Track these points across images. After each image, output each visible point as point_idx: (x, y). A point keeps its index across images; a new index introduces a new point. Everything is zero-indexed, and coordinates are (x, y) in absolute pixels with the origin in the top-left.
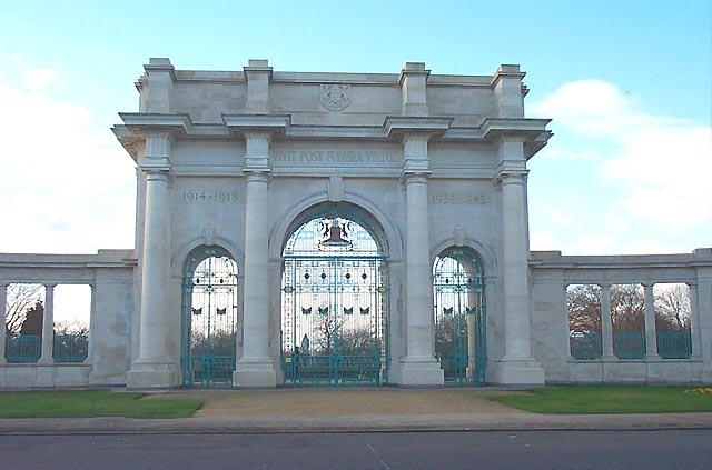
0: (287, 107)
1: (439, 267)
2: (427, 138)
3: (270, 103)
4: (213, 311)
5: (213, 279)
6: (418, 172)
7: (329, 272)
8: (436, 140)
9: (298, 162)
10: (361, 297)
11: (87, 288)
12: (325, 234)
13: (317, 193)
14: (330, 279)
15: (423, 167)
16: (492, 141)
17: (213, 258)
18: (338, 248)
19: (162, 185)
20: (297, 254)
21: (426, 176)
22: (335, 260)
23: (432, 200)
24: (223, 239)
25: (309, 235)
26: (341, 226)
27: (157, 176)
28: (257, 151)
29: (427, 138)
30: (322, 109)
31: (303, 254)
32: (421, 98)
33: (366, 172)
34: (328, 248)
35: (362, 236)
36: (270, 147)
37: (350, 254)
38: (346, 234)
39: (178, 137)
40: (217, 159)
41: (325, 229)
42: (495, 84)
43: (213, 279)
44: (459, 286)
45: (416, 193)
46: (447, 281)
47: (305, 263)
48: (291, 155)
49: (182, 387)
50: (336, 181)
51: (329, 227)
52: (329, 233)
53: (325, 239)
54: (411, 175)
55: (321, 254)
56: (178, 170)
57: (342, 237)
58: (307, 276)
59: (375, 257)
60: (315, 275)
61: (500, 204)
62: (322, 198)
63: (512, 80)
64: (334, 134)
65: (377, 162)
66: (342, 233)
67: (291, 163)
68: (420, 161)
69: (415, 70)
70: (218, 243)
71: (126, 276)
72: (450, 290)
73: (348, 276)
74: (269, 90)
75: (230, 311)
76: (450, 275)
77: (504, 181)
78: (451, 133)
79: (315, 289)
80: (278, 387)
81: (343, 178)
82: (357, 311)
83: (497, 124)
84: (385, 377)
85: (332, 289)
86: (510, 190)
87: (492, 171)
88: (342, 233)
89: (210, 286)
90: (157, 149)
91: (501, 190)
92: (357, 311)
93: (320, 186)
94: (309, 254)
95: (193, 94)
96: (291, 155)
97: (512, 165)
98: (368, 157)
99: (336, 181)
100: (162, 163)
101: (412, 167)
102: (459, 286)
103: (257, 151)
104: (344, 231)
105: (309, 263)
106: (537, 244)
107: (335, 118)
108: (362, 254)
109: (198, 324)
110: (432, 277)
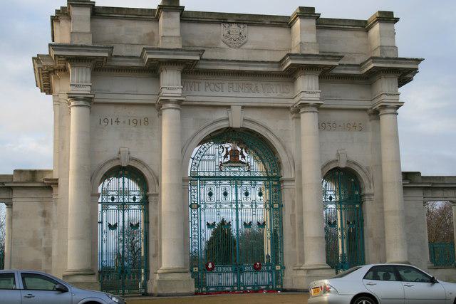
0: (198, 43)
2: (182, 68)
3: (183, 36)
5: (126, 198)
6: (312, 103)
8: (326, 75)
9: (205, 92)
10: (258, 212)
12: (226, 157)
13: (219, 120)
14: (232, 197)
15: (315, 98)
16: (368, 78)
17: (126, 179)
18: (237, 169)
19: (86, 110)
20: (202, 174)
21: (317, 106)
22: (237, 180)
23: (322, 126)
24: (136, 160)
25: (211, 157)
27: (81, 103)
28: (171, 81)
29: (182, 68)
30: (223, 45)
31: (207, 174)
32: (311, 37)
33: (263, 102)
36: (182, 78)
37: (247, 174)
38: (244, 157)
39: (101, 66)
40: (136, 90)
41: (225, 152)
42: (370, 27)
45: (308, 120)
47: (209, 183)
48: (197, 84)
49: (196, 293)
50: (236, 110)
51: (229, 150)
52: (229, 156)
53: (226, 160)
54: (167, 101)
55: (223, 174)
56: (98, 98)
57: (240, 159)
58: (225, 194)
61: (377, 131)
62: (224, 125)
64: (237, 68)
65: (273, 94)
66: (240, 156)
67: (196, 93)
68: (313, 93)
69: (307, 13)
70: (132, 164)
71: (43, 195)
73: (210, 194)
74: (91, 20)
77: (382, 112)
78: (203, 64)
80: (196, 293)
81: (243, 107)
83: (379, 62)
84: (145, 286)
86: (386, 119)
87: (370, 103)
88: (240, 156)
89: (124, 204)
90: (78, 79)
91: (300, 118)
93: (221, 114)
95: (110, 28)
96: (197, 84)
97: (389, 97)
98: (264, 89)
99: (236, 110)
100: (86, 90)
101: (166, 93)
103: (171, 81)
104: (242, 154)
105: (211, 182)
106: (407, 167)
107: (234, 54)
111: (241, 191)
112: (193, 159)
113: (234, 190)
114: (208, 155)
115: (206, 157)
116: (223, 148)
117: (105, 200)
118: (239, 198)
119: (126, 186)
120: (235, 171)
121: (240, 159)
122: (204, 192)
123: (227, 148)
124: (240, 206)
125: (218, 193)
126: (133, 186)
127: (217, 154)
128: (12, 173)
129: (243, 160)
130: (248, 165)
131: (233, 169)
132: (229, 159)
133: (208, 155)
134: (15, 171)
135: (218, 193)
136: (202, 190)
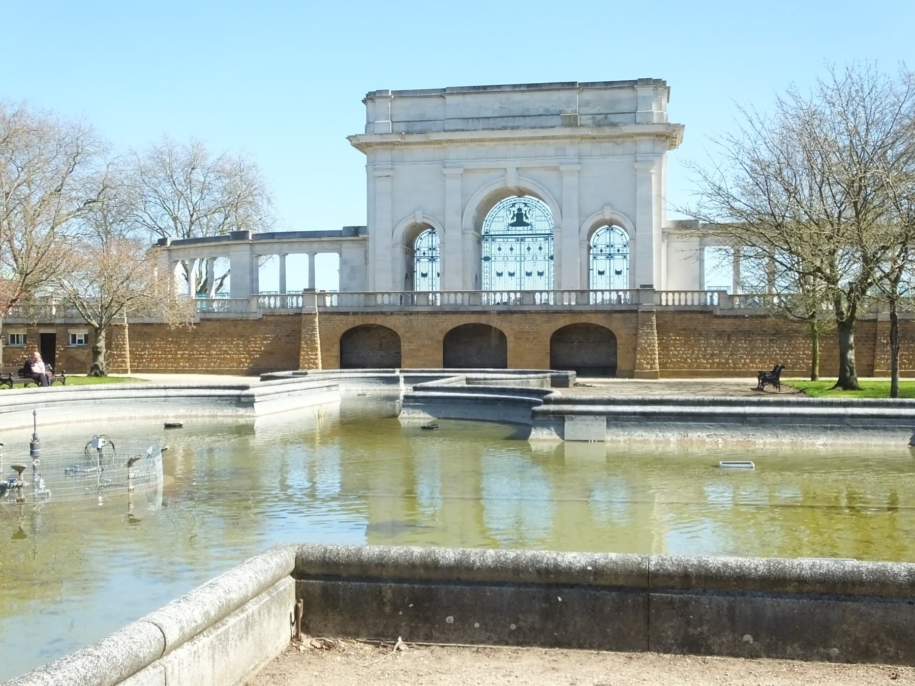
1: (617, 231)
4: (613, 273)
5: (434, 252)
7: (516, 246)
11: (335, 257)
12: (513, 218)
14: (516, 251)
18: (521, 228)
22: (521, 239)
25: (501, 219)
26: (524, 212)
34: (514, 228)
35: (539, 218)
37: (530, 232)
38: (527, 218)
43: (612, 249)
44: (432, 257)
46: (601, 251)
47: (498, 240)
51: (516, 213)
53: (513, 221)
55: (510, 233)
59: (548, 234)
60: (506, 248)
63: (501, 94)
72: (426, 260)
75: (625, 272)
76: (426, 249)
79: (506, 259)
82: (535, 274)
85: (518, 259)
89: (610, 254)
92: (535, 274)
94: (501, 233)
102: (432, 257)
104: (525, 215)
105: (513, 240)
108: (539, 232)
109: (422, 285)
110: (590, 248)
111: (525, 246)
113: (518, 246)
114: (498, 217)
115: (496, 219)
117: (418, 255)
118: (522, 253)
119: (612, 240)
120: (520, 230)
121: (524, 220)
122: (495, 246)
124: (523, 259)
125: (506, 248)
126: (423, 242)
128: (341, 229)
129: (527, 221)
131: (518, 228)
132: (515, 220)
133: (498, 217)
134: (344, 228)
135: (535, 248)
136: (493, 246)
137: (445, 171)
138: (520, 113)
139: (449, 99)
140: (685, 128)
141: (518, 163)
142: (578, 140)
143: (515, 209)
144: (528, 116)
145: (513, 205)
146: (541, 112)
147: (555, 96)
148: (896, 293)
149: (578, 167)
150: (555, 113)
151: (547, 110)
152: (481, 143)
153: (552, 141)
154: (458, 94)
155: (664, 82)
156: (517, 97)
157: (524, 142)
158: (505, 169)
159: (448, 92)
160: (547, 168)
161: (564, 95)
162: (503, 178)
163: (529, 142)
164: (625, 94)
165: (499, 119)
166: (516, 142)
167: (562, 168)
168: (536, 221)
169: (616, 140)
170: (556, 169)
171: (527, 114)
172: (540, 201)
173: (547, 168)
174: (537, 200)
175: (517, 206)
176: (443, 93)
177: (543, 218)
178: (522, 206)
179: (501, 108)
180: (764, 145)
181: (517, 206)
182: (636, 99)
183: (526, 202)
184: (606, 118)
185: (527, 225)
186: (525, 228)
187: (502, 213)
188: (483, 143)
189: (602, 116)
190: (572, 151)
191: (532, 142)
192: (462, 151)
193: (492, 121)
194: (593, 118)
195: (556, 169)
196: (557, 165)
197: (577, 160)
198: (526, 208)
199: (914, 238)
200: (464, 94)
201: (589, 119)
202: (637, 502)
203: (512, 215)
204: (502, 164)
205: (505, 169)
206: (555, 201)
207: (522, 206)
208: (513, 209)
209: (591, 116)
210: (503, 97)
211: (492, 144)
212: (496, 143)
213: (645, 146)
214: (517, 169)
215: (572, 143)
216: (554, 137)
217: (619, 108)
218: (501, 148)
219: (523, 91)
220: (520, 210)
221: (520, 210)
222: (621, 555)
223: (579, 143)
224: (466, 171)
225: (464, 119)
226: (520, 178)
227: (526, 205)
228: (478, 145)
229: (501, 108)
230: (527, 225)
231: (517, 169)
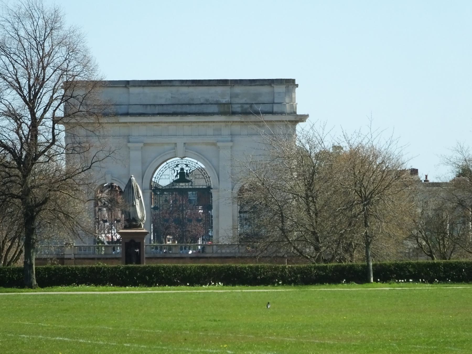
12: (176, 176)
18: (183, 184)
25: (167, 177)
26: (185, 171)
34: (178, 184)
51: (179, 171)
52: (178, 176)
53: (176, 179)
112: (197, 163)
114: (165, 175)
115: (163, 177)
116: (175, 171)
121: (186, 178)
123: (177, 171)
127: (171, 174)
129: (188, 178)
130: (191, 182)
131: (181, 184)
132: (178, 178)
133: (165, 175)
136: (161, 198)
137: (129, 145)
138: (186, 102)
139: (132, 90)
140: (309, 116)
141: (185, 140)
142: (231, 124)
143: (178, 169)
144: (193, 104)
145: (177, 166)
146: (202, 101)
147: (213, 90)
148: (296, 200)
149: (231, 144)
150: (213, 102)
151: (207, 100)
152: (157, 124)
153: (211, 124)
154: (139, 86)
155: (294, 81)
156: (184, 89)
157: (189, 124)
158: (176, 144)
159: (131, 84)
160: (207, 144)
161: (219, 89)
162: (174, 151)
163: (194, 124)
164: (265, 89)
165: (171, 106)
166: (199, 124)
167: (219, 144)
168: (196, 178)
169: (259, 123)
170: (214, 144)
171: (192, 102)
172: (168, 162)
173: (207, 144)
174: (165, 163)
175: (180, 166)
176: (127, 84)
177: (201, 176)
178: (184, 166)
179: (172, 97)
180: (85, 153)
181: (180, 166)
182: (273, 93)
183: (187, 163)
184: (251, 107)
185: (188, 181)
186: (187, 184)
187: (168, 172)
188: (159, 124)
189: (248, 106)
190: (226, 131)
191: (196, 124)
192: (143, 130)
193: (165, 108)
194: (242, 107)
195: (214, 144)
196: (214, 142)
197: (230, 139)
198: (187, 168)
199: (471, 198)
200: (143, 86)
201: (238, 107)
202: (17, 62)
203: (176, 173)
204: (173, 140)
205: (176, 144)
206: (213, 169)
207: (184, 166)
208: (177, 169)
209: (240, 105)
210: (174, 89)
211: (166, 124)
212: (169, 124)
213: (280, 130)
214: (184, 144)
215: (226, 126)
216: (214, 122)
217: (261, 99)
218: (172, 129)
219: (188, 86)
220: (182, 169)
221: (182, 169)
222: (155, 265)
223: (231, 125)
224: (145, 144)
225: (144, 105)
226: (187, 150)
227: (187, 165)
228: (154, 126)
229: (172, 97)
230: (188, 181)
231: (184, 144)
